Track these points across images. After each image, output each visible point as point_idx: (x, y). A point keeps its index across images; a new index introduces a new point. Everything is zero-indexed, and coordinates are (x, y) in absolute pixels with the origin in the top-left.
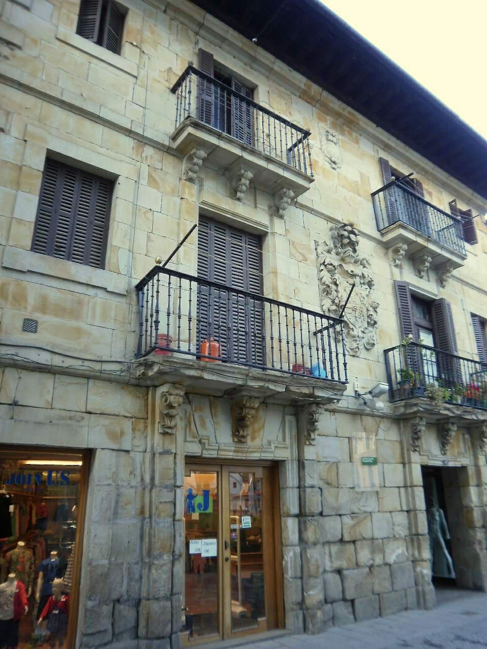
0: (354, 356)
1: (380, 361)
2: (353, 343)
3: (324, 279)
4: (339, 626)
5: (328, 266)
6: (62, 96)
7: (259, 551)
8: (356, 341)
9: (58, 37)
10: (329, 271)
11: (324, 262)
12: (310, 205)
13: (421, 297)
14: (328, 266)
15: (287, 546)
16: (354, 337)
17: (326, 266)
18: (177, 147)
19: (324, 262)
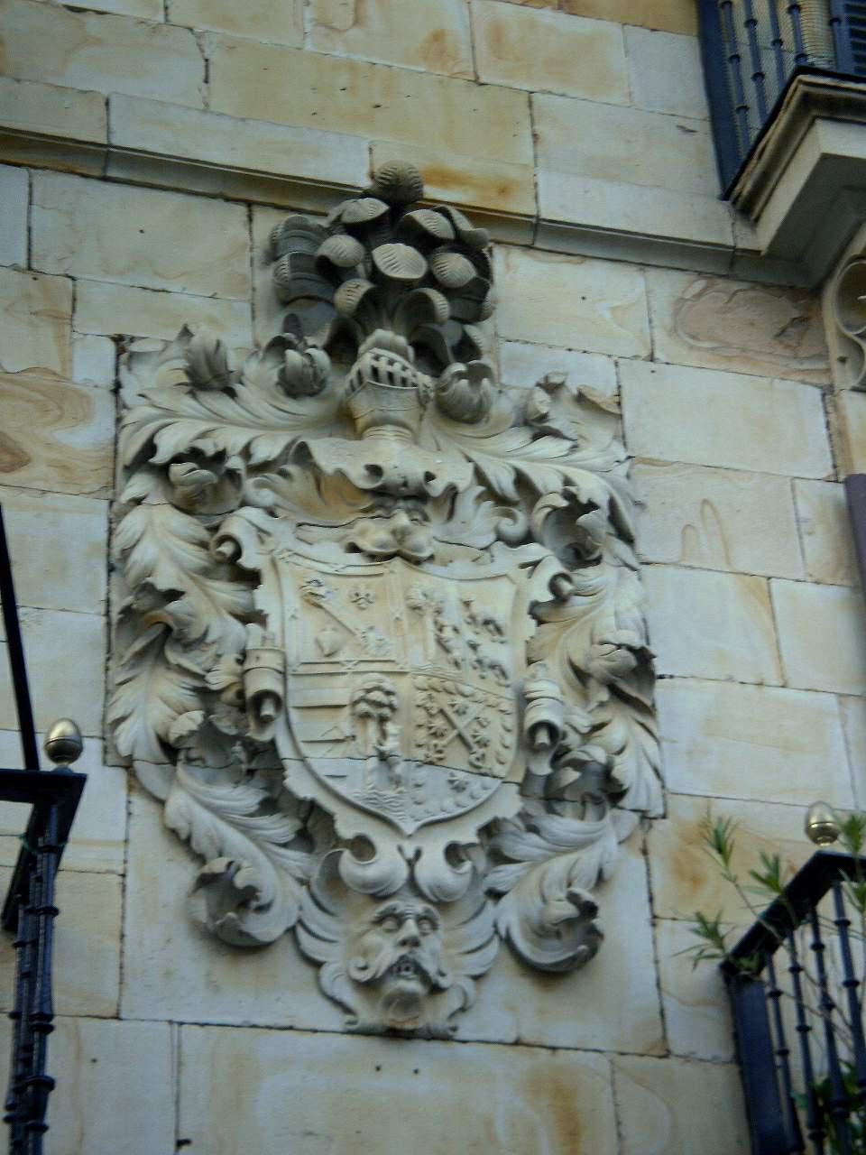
0: (393, 1034)
1: (678, 1043)
2: (374, 938)
3: (140, 556)
4: (538, 412)
5: (178, 470)
6: (109, 132)
7: (478, 358)
8: (400, 920)
9: (303, 661)
10: (188, 506)
11: (150, 448)
12: (85, 128)
13: (740, 1095)
14: (178, 470)
15: (714, 1061)
16: (378, 894)
17: (163, 471)
18: (772, 245)
19: (150, 448)
